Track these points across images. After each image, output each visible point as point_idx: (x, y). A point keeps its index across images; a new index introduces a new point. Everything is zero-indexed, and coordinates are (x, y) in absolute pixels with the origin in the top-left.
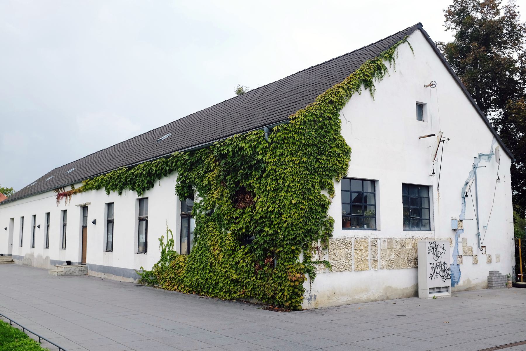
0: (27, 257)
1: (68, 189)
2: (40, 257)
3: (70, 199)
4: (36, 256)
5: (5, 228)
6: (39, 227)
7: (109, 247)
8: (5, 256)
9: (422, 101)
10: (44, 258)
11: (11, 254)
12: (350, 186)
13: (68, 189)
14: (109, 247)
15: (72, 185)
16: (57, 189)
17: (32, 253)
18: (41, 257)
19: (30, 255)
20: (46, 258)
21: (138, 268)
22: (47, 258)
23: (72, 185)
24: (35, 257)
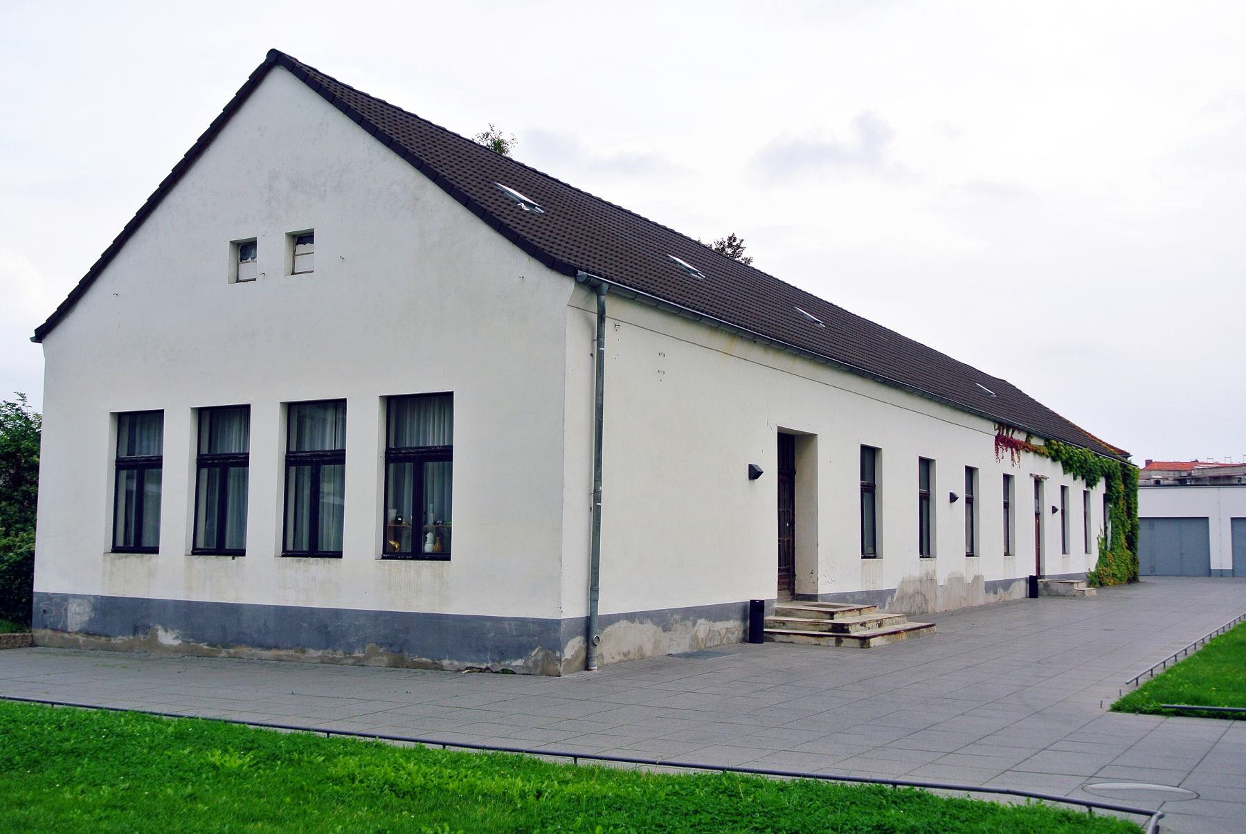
0: (910, 590)
1: (1020, 437)
2: (956, 580)
3: (1019, 457)
4: (941, 580)
5: (745, 472)
6: (1054, 510)
7: (870, 548)
8: (1054, 587)
9: (796, 424)
10: (970, 580)
11: (1231, 572)
12: (1085, 507)
13: (1020, 437)
14: (870, 548)
15: (1029, 435)
16: (1002, 425)
17: (928, 573)
18: (960, 579)
19: (921, 581)
20: (973, 581)
21: (1087, 571)
22: (977, 578)
23: (1029, 435)
24: (940, 583)
